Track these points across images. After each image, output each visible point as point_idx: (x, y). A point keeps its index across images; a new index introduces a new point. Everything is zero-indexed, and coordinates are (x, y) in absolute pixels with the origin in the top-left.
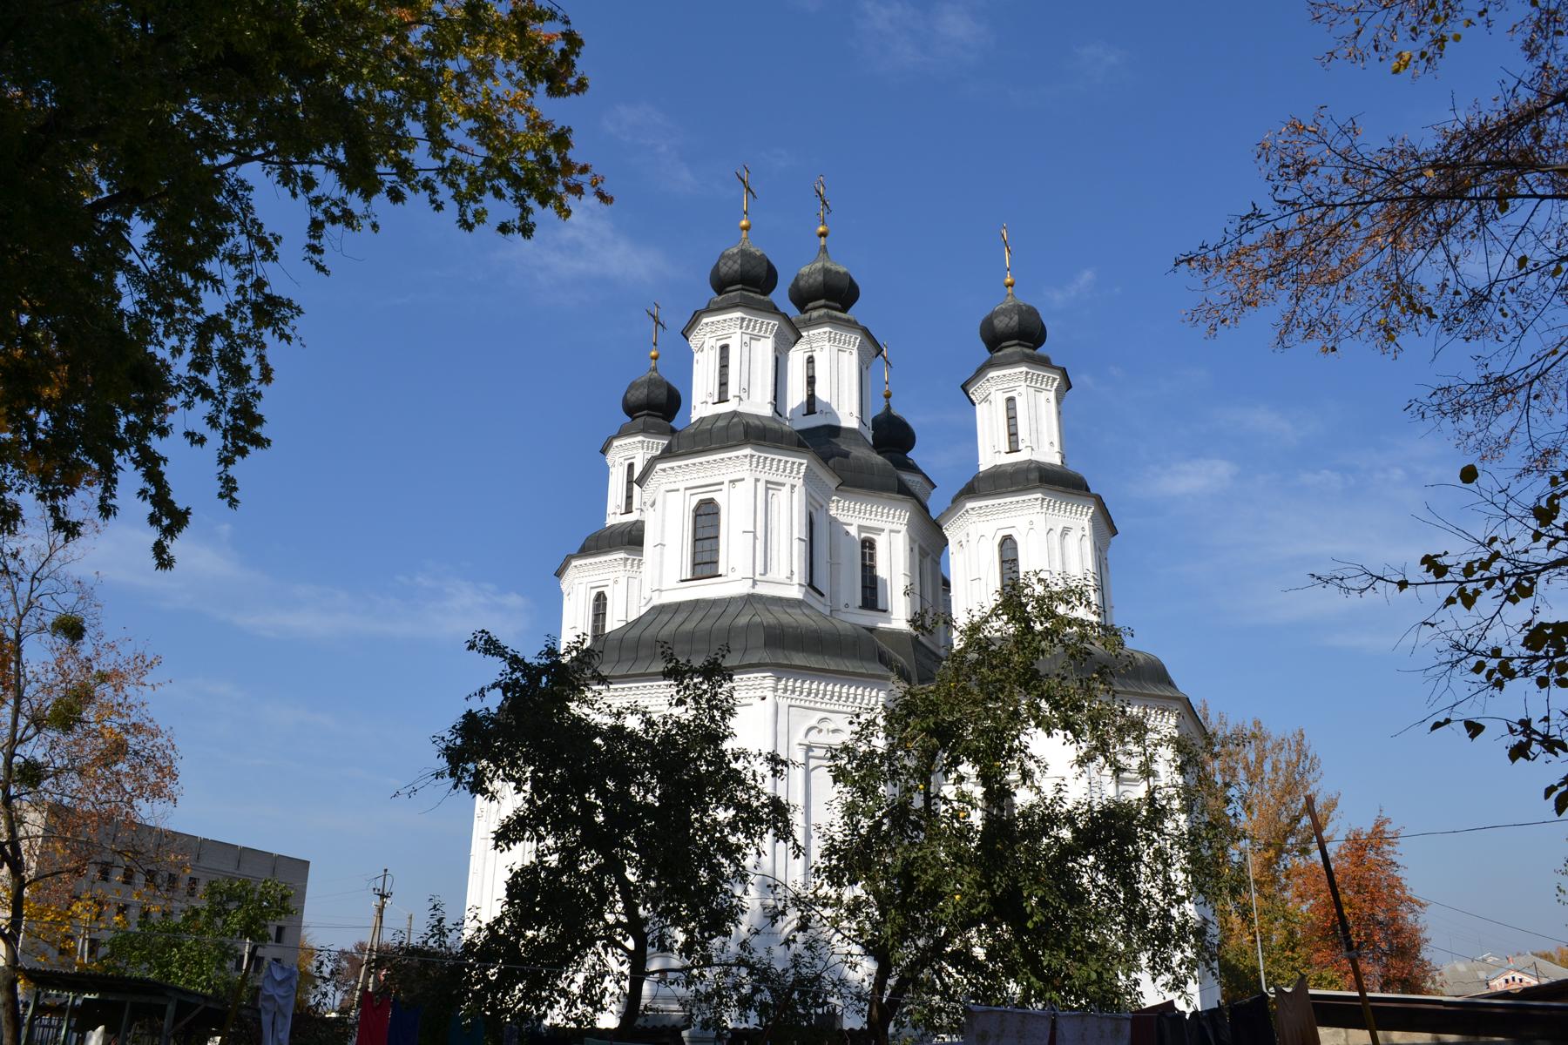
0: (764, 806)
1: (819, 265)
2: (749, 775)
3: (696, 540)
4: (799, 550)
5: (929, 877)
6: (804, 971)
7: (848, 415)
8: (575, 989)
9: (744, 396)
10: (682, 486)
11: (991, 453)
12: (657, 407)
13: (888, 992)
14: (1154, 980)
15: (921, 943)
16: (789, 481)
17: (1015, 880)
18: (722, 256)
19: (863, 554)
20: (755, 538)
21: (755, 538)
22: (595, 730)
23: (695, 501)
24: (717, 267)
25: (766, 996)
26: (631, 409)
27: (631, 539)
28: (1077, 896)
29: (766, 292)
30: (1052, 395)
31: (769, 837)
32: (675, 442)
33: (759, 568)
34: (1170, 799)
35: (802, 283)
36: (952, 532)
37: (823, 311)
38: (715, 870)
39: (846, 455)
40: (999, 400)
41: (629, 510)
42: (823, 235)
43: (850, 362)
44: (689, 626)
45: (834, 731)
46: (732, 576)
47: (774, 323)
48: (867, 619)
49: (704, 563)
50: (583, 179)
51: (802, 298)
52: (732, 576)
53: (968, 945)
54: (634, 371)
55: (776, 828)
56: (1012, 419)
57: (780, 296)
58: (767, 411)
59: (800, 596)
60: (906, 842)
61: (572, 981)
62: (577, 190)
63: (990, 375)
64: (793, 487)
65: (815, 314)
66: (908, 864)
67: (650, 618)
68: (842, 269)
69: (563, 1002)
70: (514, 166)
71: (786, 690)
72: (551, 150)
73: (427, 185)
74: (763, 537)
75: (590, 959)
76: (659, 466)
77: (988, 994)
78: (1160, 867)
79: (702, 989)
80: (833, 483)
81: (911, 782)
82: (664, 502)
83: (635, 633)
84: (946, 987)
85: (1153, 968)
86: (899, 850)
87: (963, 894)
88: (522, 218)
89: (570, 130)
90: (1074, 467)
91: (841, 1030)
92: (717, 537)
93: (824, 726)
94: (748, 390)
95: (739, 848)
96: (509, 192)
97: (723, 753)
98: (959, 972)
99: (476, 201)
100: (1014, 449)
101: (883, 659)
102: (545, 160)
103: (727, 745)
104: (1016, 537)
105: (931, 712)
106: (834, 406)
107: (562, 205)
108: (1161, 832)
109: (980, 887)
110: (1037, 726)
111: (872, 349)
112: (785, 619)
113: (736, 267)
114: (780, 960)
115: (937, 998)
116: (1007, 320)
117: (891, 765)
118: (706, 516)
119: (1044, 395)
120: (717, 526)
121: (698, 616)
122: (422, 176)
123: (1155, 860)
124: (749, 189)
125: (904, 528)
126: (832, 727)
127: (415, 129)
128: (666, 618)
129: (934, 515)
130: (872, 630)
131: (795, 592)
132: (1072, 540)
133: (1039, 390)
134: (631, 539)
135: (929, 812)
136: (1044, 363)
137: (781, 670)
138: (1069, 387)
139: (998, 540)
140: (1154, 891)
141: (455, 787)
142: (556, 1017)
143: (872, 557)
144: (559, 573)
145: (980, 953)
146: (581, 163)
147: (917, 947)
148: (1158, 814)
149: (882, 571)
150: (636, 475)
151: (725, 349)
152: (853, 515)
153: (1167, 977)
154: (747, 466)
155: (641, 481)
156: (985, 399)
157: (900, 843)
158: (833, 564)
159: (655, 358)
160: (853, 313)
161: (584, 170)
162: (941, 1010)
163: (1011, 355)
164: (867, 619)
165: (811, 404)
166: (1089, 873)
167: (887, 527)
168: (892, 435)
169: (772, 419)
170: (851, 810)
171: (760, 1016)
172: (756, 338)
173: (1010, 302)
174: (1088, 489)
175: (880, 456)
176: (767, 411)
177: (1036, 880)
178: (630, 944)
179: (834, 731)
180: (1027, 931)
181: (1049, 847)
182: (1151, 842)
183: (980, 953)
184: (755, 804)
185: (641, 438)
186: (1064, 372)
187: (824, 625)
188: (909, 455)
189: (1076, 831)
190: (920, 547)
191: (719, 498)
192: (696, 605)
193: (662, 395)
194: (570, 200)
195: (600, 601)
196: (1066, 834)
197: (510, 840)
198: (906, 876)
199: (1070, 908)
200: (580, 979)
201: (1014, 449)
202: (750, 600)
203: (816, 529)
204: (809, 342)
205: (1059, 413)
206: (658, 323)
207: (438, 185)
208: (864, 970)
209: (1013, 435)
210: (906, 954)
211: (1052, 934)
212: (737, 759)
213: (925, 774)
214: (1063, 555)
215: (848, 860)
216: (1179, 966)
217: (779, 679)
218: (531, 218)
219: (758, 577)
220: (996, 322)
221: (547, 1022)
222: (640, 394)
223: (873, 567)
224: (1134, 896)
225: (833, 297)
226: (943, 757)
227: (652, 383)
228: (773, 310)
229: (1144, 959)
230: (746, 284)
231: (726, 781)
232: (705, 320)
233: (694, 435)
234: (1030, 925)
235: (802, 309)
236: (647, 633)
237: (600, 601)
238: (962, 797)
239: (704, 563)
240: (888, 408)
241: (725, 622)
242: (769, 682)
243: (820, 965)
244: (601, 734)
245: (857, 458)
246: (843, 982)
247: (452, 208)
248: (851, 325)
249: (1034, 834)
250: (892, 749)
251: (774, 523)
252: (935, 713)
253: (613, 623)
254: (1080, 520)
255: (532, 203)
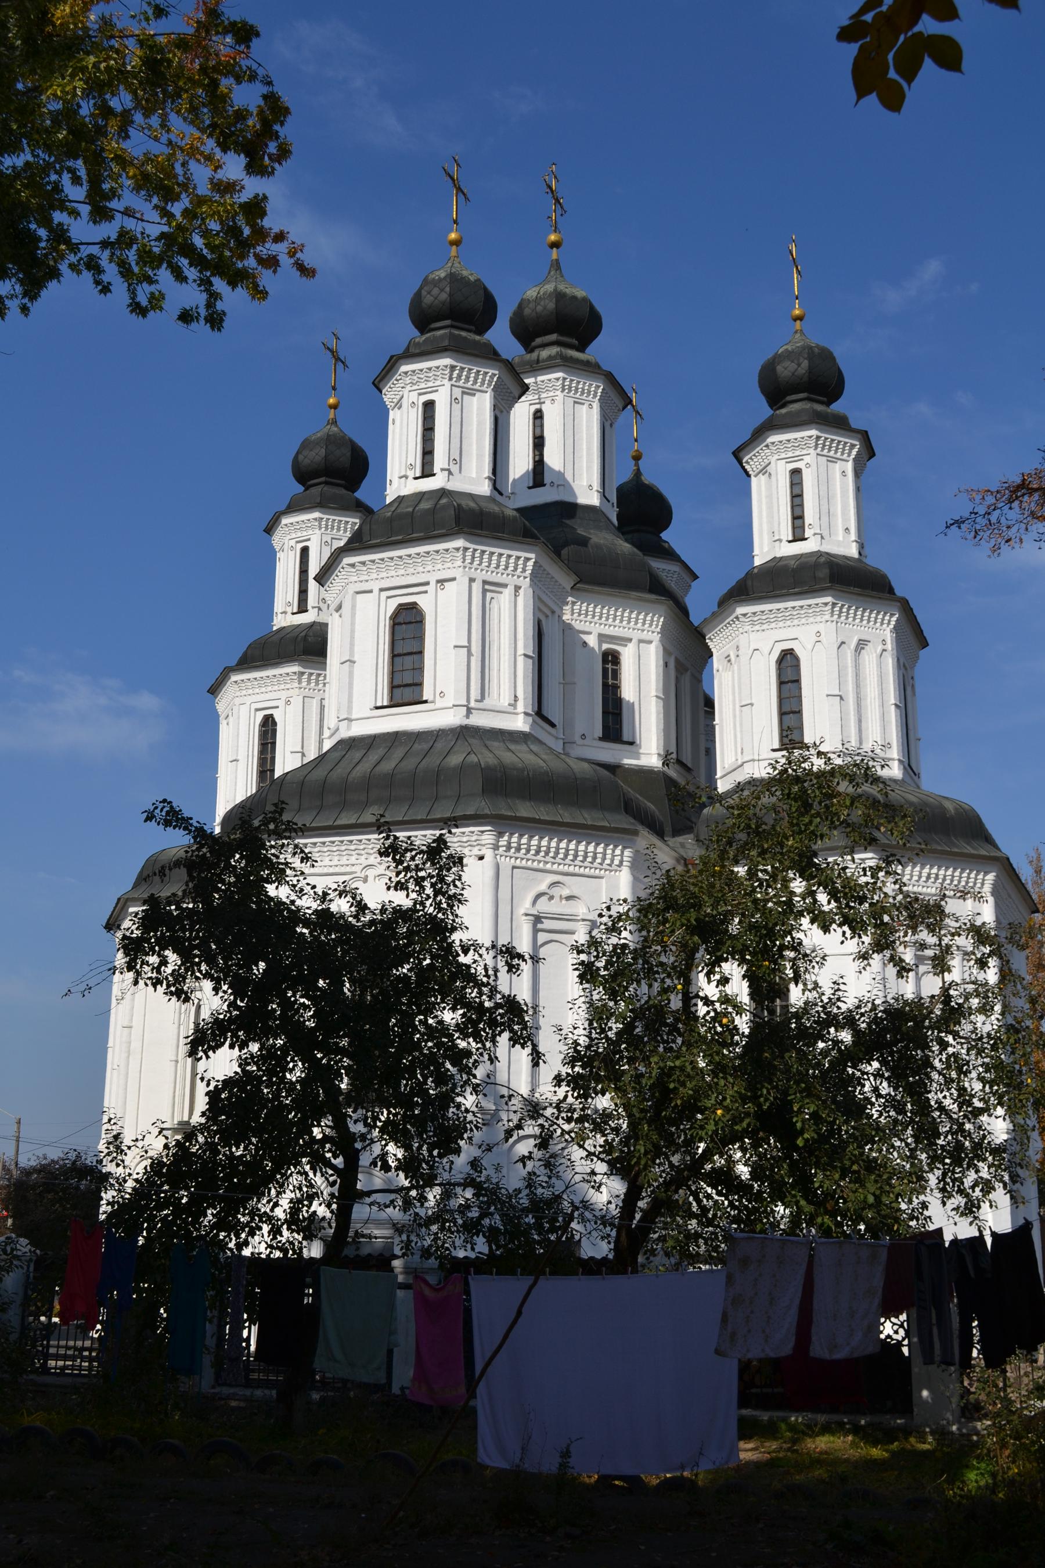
0: (498, 1006)
1: (549, 287)
2: (480, 970)
3: (394, 656)
4: (524, 669)
5: (687, 1091)
6: (540, 1191)
7: (587, 488)
8: (279, 1213)
9: (455, 469)
10: (376, 586)
11: (770, 542)
12: (338, 473)
13: (638, 1216)
14: (944, 1204)
15: (675, 1159)
16: (512, 581)
17: (785, 1093)
18: (426, 282)
19: (605, 671)
20: (470, 654)
21: (470, 654)
22: (296, 916)
23: (392, 605)
24: (418, 296)
25: (497, 1221)
26: (303, 475)
27: (309, 647)
28: (857, 1109)
29: (481, 331)
30: (849, 467)
31: (504, 1039)
32: (366, 528)
33: (475, 693)
34: (967, 997)
35: (527, 311)
36: (718, 643)
37: (554, 350)
38: (442, 1078)
39: (584, 542)
40: (781, 472)
41: (302, 608)
42: (555, 245)
43: (590, 417)
44: (387, 766)
45: (569, 898)
46: (440, 703)
47: (492, 372)
48: (608, 753)
49: (405, 685)
50: (280, 249)
51: (527, 331)
52: (440, 703)
53: (731, 1162)
54: (304, 424)
55: (512, 1031)
56: (797, 498)
57: (500, 335)
58: (484, 488)
59: (526, 728)
60: (661, 1049)
61: (276, 1205)
62: (271, 262)
63: (770, 440)
64: (517, 588)
65: (545, 353)
66: (666, 1074)
67: (337, 755)
68: (580, 293)
69: (266, 1228)
70: (198, 241)
71: (509, 847)
72: (241, 220)
73: (92, 265)
74: (479, 653)
75: (295, 1180)
76: (347, 560)
77: (752, 1220)
78: (954, 1075)
79: (422, 1212)
80: (566, 581)
81: (668, 982)
82: (354, 607)
83: (320, 773)
84: (704, 1210)
85: (943, 1190)
86: (654, 1059)
87: (727, 1109)
88: (209, 305)
89: (265, 197)
90: (874, 562)
91: (580, 1259)
92: (421, 653)
93: (556, 891)
94: (459, 462)
95: (468, 1053)
96: (192, 274)
97: (450, 945)
98: (719, 1193)
99: (150, 281)
100: (798, 536)
101: (630, 808)
102: (234, 231)
103: (456, 937)
104: (799, 652)
105: (693, 906)
106: (569, 477)
107: (256, 286)
108: (956, 1035)
109: (744, 1100)
110: (812, 922)
111: (618, 400)
112: (508, 758)
113: (444, 296)
114: (514, 1179)
115: (694, 1222)
116: (793, 366)
117: (646, 962)
118: (407, 625)
119: (838, 467)
120: (420, 638)
121: (399, 753)
122: (85, 251)
123: (949, 1067)
124: (459, 190)
125: (656, 638)
126: (566, 892)
127: (76, 193)
128: (358, 755)
129: (696, 619)
130: (613, 768)
131: (520, 723)
132: (870, 656)
133: (832, 460)
134: (309, 647)
135: (688, 1012)
136: (839, 424)
137: (503, 823)
138: (872, 454)
139: (776, 655)
140: (947, 1102)
141: (136, 983)
142: (259, 1246)
143: (616, 674)
144: (214, 690)
145: (743, 1171)
146: (276, 230)
147: (671, 1165)
148: (953, 1014)
149: (628, 692)
150: (313, 569)
151: (429, 407)
152: (592, 621)
153: (958, 1200)
154: (459, 563)
155: (322, 578)
156: (763, 471)
157: (654, 1051)
158: (567, 684)
159: (335, 407)
160: (595, 351)
161: (280, 237)
162: (697, 1235)
163: (799, 413)
164: (608, 753)
165: (539, 471)
166: (873, 1081)
167: (636, 635)
168: (641, 509)
169: (490, 499)
170: (598, 1015)
171: (489, 1243)
172: (471, 392)
173: (798, 342)
174: (891, 591)
175: (624, 543)
176: (484, 488)
177: (809, 1093)
178: (339, 1162)
179: (569, 898)
180: (797, 1149)
181: (825, 1053)
182: (944, 1045)
183: (743, 1171)
184: (487, 1004)
185: (317, 514)
186: (865, 437)
187: (556, 765)
188: (664, 535)
189: (857, 1033)
190: (677, 662)
191: (424, 602)
192: (395, 738)
193: (344, 456)
194: (266, 278)
195: (268, 728)
196: (846, 1036)
197: (210, 1048)
198: (662, 1091)
199: (847, 1122)
200: (285, 1203)
201: (798, 536)
202: (463, 733)
203: (547, 642)
204: (538, 392)
205: (858, 489)
206: (338, 359)
207: (104, 263)
208: (607, 1193)
209: (798, 517)
210: (659, 1171)
211: (828, 1151)
212: (466, 951)
213: (685, 975)
214: (857, 675)
215: (590, 1069)
216: (973, 1188)
217: (500, 834)
218: (220, 306)
219: (473, 704)
220: (779, 368)
221: (247, 1252)
222: (316, 456)
223: (617, 687)
224: (923, 1108)
225: (566, 331)
226: (702, 955)
227: (333, 441)
228: (489, 355)
229: (933, 1179)
230: (454, 320)
231: (450, 976)
232: (404, 368)
233: (391, 520)
234: (800, 1142)
235: (529, 348)
236: (335, 775)
237: (268, 728)
238: (726, 1000)
239: (405, 685)
240: (638, 473)
241: (432, 762)
242: (488, 838)
243: (559, 1186)
244: (307, 923)
245: (598, 547)
246: (586, 1205)
247: (120, 287)
248: (591, 369)
249: (811, 1036)
250: (646, 942)
251: (493, 635)
252: (698, 906)
253: (286, 762)
254: (881, 630)
255: (219, 284)
